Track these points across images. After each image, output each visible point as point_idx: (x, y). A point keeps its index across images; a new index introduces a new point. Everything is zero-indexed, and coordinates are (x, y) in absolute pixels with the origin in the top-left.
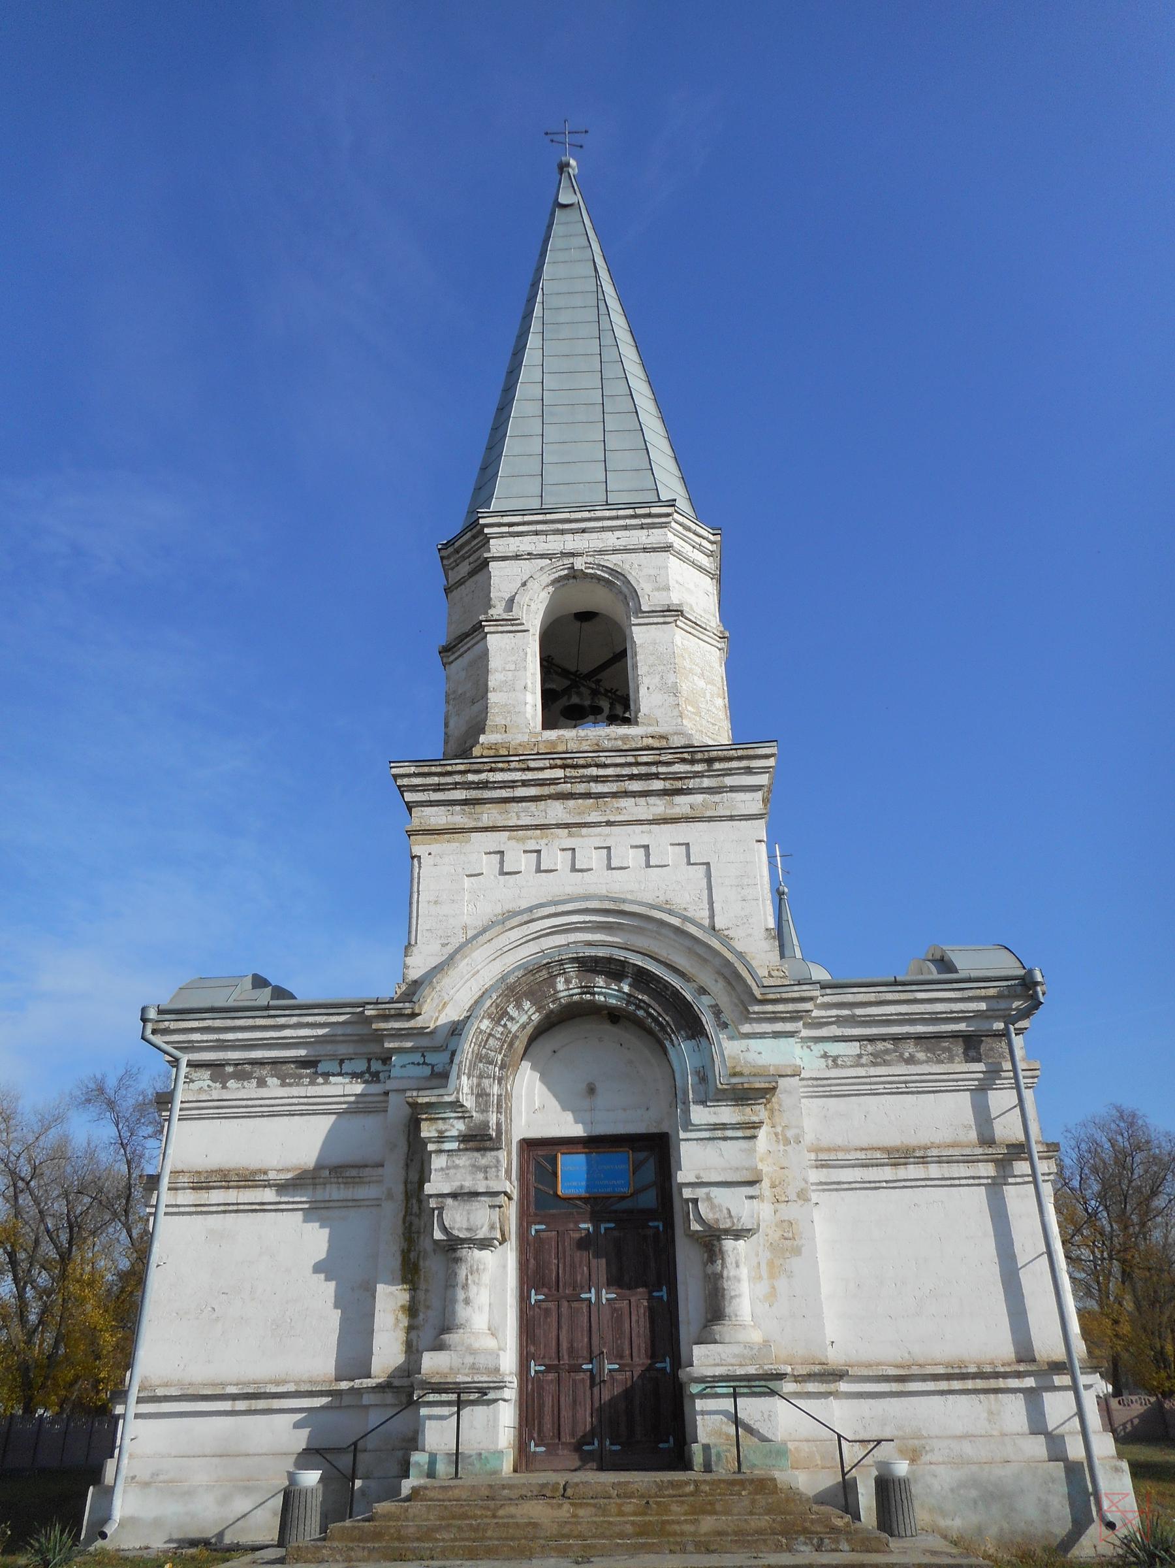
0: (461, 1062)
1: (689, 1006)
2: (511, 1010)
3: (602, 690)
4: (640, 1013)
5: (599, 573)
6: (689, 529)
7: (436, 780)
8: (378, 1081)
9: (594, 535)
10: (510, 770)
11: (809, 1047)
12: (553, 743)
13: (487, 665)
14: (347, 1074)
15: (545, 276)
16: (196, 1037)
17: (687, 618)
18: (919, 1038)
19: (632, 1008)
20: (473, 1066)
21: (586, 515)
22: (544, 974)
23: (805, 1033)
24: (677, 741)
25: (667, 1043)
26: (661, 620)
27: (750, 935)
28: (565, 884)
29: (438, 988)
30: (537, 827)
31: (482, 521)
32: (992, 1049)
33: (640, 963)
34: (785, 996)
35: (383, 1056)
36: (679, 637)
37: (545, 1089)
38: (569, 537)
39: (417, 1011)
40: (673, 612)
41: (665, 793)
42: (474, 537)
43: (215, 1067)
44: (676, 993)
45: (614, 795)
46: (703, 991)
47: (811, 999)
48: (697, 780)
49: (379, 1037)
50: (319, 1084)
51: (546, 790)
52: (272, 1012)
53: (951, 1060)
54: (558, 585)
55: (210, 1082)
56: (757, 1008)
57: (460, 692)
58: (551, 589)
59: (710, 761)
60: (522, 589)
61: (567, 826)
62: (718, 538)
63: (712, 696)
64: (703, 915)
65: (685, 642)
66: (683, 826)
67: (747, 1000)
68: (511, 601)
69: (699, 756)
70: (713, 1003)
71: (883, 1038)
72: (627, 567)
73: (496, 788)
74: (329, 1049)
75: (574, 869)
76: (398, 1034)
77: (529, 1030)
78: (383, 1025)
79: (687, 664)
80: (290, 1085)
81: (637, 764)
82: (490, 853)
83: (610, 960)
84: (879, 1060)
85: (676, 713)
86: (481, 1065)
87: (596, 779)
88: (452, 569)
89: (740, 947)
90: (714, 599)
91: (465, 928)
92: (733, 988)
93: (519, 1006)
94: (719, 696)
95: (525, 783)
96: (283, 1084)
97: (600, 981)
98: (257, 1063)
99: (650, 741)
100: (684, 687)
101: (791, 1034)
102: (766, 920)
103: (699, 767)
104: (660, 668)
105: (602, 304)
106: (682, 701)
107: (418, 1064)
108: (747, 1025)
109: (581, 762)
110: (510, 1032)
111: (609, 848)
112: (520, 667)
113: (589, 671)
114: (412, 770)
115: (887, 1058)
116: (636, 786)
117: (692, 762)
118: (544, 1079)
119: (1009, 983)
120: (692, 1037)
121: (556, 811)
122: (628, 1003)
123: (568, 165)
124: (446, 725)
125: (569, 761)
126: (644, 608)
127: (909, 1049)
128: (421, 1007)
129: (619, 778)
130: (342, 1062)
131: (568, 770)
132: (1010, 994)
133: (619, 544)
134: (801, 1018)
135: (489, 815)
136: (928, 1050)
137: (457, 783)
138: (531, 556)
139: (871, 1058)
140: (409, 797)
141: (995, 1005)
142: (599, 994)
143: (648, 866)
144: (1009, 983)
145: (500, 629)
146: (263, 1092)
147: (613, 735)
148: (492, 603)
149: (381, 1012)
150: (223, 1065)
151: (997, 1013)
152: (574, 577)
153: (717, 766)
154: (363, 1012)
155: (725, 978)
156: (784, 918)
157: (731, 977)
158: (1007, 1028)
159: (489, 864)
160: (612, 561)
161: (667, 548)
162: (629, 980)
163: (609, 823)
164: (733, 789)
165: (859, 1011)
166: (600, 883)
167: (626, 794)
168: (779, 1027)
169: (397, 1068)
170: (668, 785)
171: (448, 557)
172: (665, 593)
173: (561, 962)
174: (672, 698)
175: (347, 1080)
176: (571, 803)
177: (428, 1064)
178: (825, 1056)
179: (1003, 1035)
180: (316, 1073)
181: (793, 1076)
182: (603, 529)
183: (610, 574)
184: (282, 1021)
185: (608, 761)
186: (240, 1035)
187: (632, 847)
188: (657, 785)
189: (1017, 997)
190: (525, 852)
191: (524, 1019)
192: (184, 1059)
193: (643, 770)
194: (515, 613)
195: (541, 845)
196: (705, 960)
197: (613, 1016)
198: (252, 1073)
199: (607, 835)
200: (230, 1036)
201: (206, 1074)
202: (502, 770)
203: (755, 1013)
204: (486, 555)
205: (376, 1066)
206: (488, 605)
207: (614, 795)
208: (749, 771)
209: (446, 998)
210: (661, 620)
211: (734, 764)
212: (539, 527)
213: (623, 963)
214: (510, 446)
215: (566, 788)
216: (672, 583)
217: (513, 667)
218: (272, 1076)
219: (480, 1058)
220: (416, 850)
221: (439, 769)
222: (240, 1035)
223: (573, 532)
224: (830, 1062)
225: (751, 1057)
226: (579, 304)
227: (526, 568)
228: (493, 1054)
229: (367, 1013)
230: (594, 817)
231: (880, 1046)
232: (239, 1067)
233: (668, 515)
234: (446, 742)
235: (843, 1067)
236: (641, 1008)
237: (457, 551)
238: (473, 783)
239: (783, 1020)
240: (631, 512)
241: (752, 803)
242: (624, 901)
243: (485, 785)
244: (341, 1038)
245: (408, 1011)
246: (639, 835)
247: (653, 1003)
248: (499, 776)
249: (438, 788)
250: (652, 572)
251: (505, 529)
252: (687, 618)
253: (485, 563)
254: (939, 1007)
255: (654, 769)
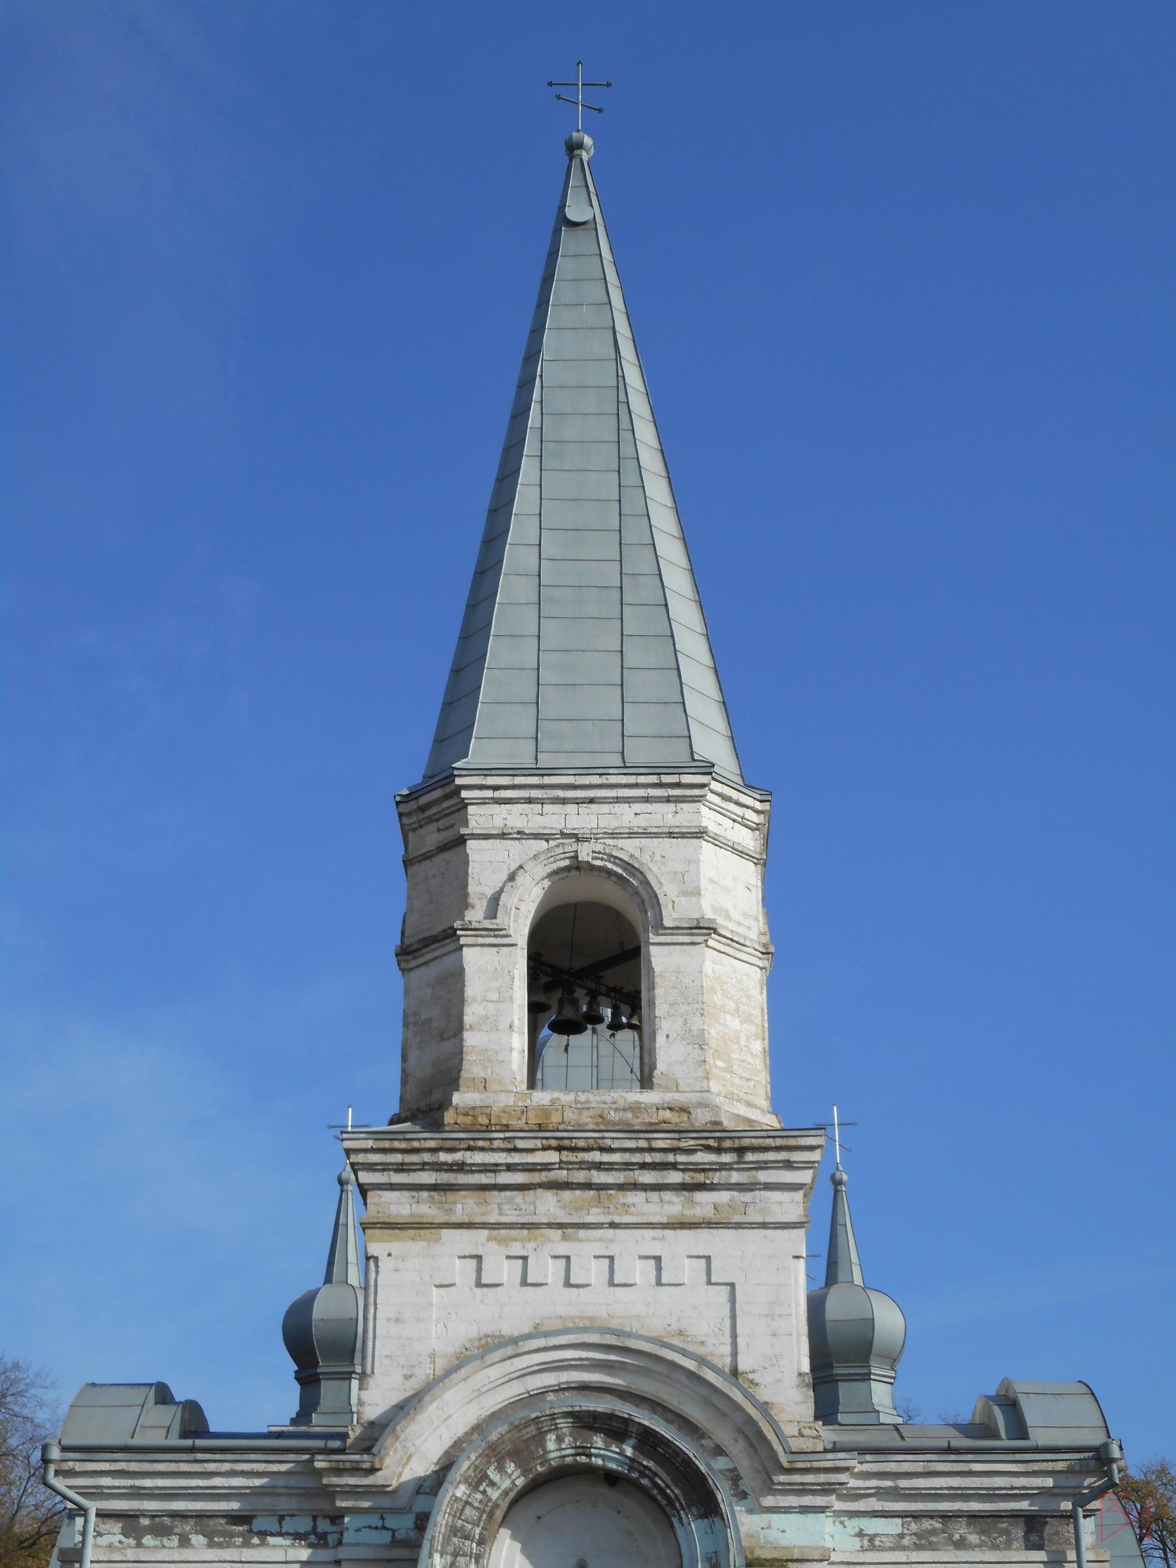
0: (434, 1537)
1: (702, 1478)
2: (492, 1473)
3: (603, 989)
4: (645, 1482)
5: (610, 866)
6: (728, 799)
7: (398, 1158)
8: (325, 1545)
9: (605, 808)
10: (492, 1150)
11: (842, 1523)
12: (545, 1111)
13: (462, 991)
14: (288, 1534)
15: (546, 354)
16: (106, 1481)
17: (720, 935)
18: (973, 1517)
19: (635, 1475)
20: (447, 1541)
21: (596, 780)
22: (532, 1430)
23: (839, 1505)
24: (701, 1118)
25: (675, 1520)
26: (687, 939)
27: (779, 1381)
28: (555, 1303)
29: (403, 1437)
30: (523, 1226)
31: (458, 781)
32: (1057, 1533)
33: (646, 1423)
34: (816, 1465)
35: (332, 1514)
36: (712, 962)
37: (526, 1562)
38: (572, 808)
39: (377, 1466)
40: (702, 929)
41: (684, 1187)
42: (447, 797)
43: (128, 1519)
44: (688, 1462)
45: (621, 1187)
46: (719, 1451)
47: (847, 1469)
48: (724, 1173)
49: (330, 1493)
50: (254, 1546)
51: (536, 1178)
52: (200, 1456)
53: (1008, 1546)
54: (556, 878)
55: (121, 1537)
56: (782, 1478)
57: (424, 1016)
58: (547, 883)
59: (741, 1151)
60: (508, 876)
61: (561, 1226)
62: (766, 806)
63: (748, 1038)
64: (720, 1352)
65: (717, 967)
66: (703, 1234)
67: (770, 1469)
68: (494, 903)
69: (728, 1144)
70: (731, 1466)
71: (930, 1515)
72: (645, 859)
73: (473, 1172)
74: (267, 1502)
75: (568, 1284)
76: (353, 1492)
77: (512, 1495)
78: (335, 1480)
79: (718, 999)
80: (220, 1546)
81: (651, 1150)
82: (465, 1257)
83: (611, 1417)
84: (923, 1542)
85: (701, 1074)
86: (455, 1540)
87: (599, 1166)
88: (414, 830)
89: (763, 1395)
90: (757, 894)
91: (433, 1356)
92: (756, 1451)
93: (501, 1469)
94: (756, 1037)
95: (510, 1168)
96: (211, 1545)
97: (598, 1441)
98: (178, 1516)
99: (667, 1114)
100: (713, 1034)
101: (821, 1510)
102: (799, 1362)
103: (726, 1158)
104: (684, 1008)
105: (623, 408)
106: (710, 1059)
107: (376, 1528)
108: (770, 1498)
109: (581, 1144)
110: (490, 1500)
111: (611, 1258)
112: (505, 998)
113: (592, 966)
114: (370, 1144)
115: (934, 1539)
116: (647, 1177)
117: (719, 1150)
118: (526, 1551)
119: (1081, 1456)
120: (703, 1516)
121: (548, 1205)
122: (631, 1469)
123: (580, 146)
124: (404, 1058)
125: (566, 1143)
126: (667, 923)
127: (960, 1530)
128: (382, 1460)
129: (627, 1166)
130: (281, 1518)
131: (564, 1153)
132: (1080, 1470)
133: (640, 823)
134: (834, 1491)
135: (464, 1206)
136: (982, 1532)
137: (425, 1164)
138: (522, 835)
139: (914, 1539)
140: (365, 1177)
141: (1063, 1481)
142: (596, 1456)
143: (659, 1283)
144: (1081, 1456)
145: (480, 940)
146: (188, 1554)
147: (621, 1103)
148: (470, 900)
149: (334, 1465)
150: (137, 1516)
151: (1066, 1491)
152: (578, 868)
153: (750, 1157)
154: (311, 1461)
155: (747, 1438)
156: (840, 1220)
157: (754, 1438)
158: (1074, 1510)
159: (464, 1271)
160: (628, 848)
161: (700, 834)
162: (633, 1441)
163: (613, 1225)
164: (768, 1187)
165: (903, 1483)
166: (599, 1303)
167: (636, 1186)
168: (808, 1500)
169: (351, 1532)
170: (688, 1178)
171: (409, 814)
172: (694, 899)
173: (553, 1417)
174: (697, 1052)
175: (288, 1542)
176: (567, 1195)
177: (387, 1529)
178: (860, 1534)
179: (1070, 1517)
180: (250, 1531)
181: (822, 1561)
182: (618, 800)
183: (625, 869)
184: (212, 1467)
185: (615, 1145)
186: (160, 1482)
187: (641, 1257)
188: (675, 1177)
189: (1089, 1473)
190: (508, 1257)
191: (507, 1484)
192: (93, 1506)
193: (658, 1157)
194: (500, 921)
195: (528, 1249)
196: (724, 1415)
197: (611, 1479)
198: (172, 1528)
199: (611, 1241)
200: (147, 1483)
201: (117, 1527)
202: (482, 1149)
203: (779, 1484)
204: (463, 831)
205: (323, 1526)
206: (464, 903)
207: (621, 1187)
208: (788, 1165)
209: (412, 1449)
210: (687, 939)
211: (771, 1156)
212: (534, 793)
213: (627, 1421)
214: (497, 652)
215: (562, 1175)
216: (704, 884)
217: (495, 997)
218: (197, 1533)
219: (454, 1531)
220: (374, 1249)
221: (403, 1145)
222: (160, 1482)
223: (578, 802)
224: (866, 1542)
225: (773, 1535)
226: (592, 410)
227: (516, 852)
228: (470, 1526)
229: (318, 1465)
230: (595, 1215)
231: (927, 1524)
232: (157, 1520)
233: (703, 786)
234: (404, 1082)
235: (881, 1549)
236: (646, 1476)
237: (422, 809)
238: (445, 1164)
239: (813, 1492)
240: (653, 779)
241: (789, 1206)
242: (629, 1335)
243: (461, 1167)
244: (283, 1491)
245: (366, 1466)
246: (649, 1242)
247: (660, 1471)
248: (478, 1158)
249: (401, 1168)
250: (680, 868)
251: (489, 794)
252: (720, 935)
253: (461, 841)
254: (998, 1482)
255: (671, 1158)
